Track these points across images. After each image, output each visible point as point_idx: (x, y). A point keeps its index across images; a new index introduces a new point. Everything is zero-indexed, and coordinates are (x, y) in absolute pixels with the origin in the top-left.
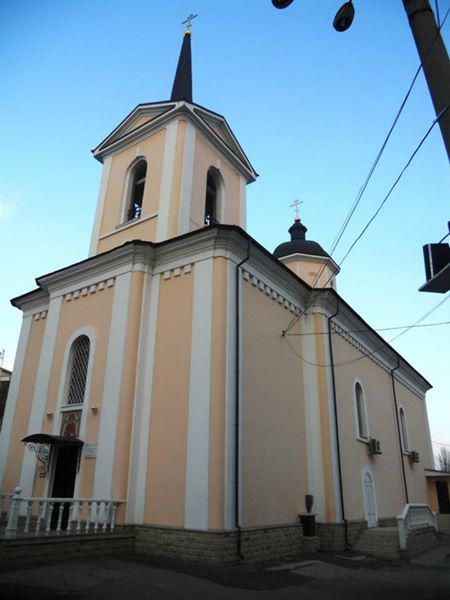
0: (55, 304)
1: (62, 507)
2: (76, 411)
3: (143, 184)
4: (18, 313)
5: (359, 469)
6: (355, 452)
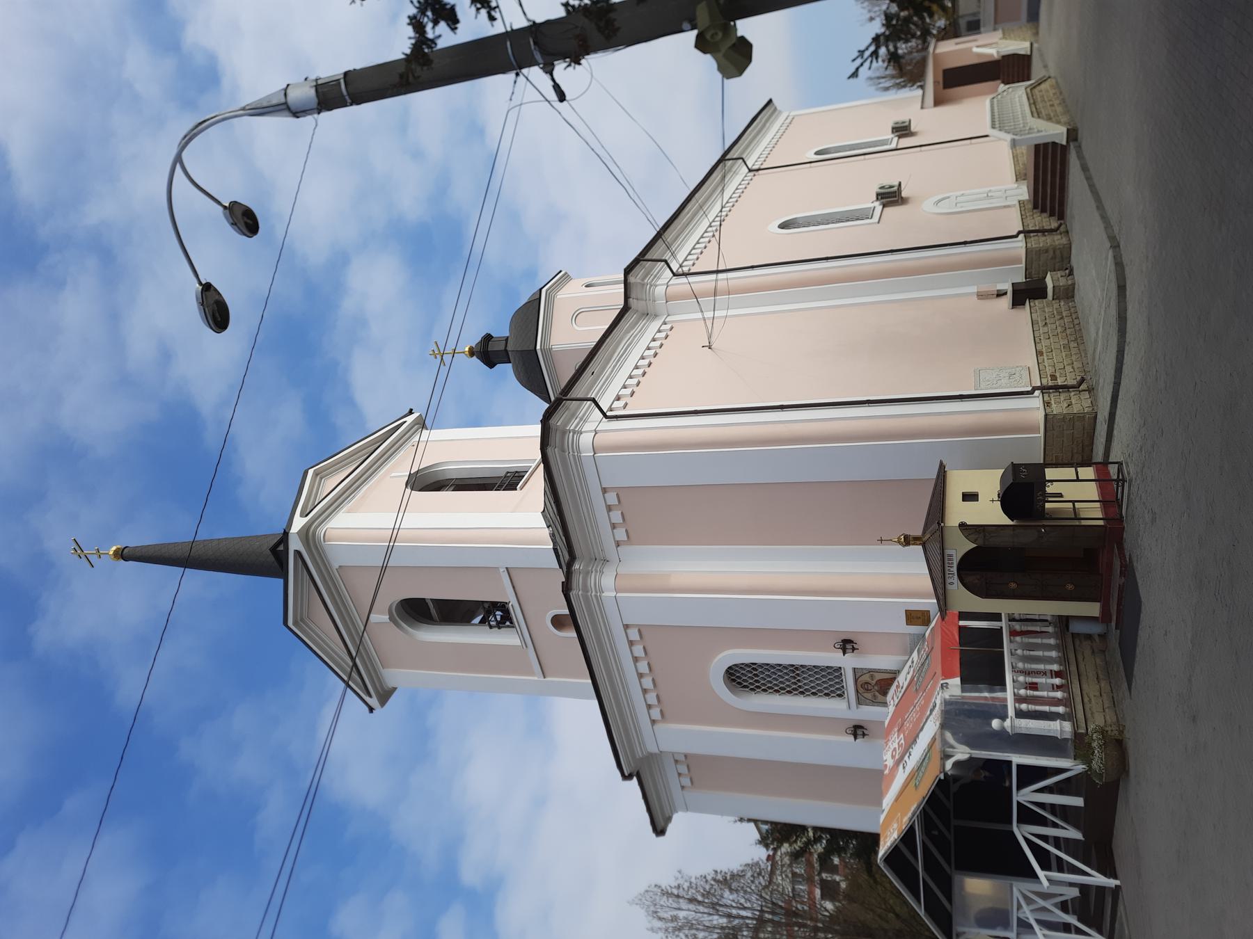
0: (671, 738)
1: (1024, 706)
2: (856, 681)
3: (439, 603)
4: (680, 822)
5: (922, 218)
6: (894, 227)
